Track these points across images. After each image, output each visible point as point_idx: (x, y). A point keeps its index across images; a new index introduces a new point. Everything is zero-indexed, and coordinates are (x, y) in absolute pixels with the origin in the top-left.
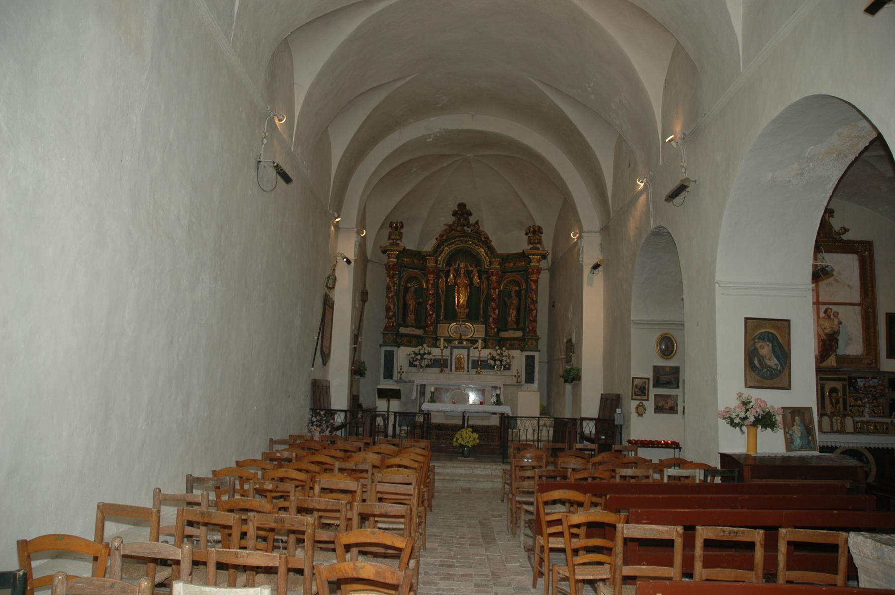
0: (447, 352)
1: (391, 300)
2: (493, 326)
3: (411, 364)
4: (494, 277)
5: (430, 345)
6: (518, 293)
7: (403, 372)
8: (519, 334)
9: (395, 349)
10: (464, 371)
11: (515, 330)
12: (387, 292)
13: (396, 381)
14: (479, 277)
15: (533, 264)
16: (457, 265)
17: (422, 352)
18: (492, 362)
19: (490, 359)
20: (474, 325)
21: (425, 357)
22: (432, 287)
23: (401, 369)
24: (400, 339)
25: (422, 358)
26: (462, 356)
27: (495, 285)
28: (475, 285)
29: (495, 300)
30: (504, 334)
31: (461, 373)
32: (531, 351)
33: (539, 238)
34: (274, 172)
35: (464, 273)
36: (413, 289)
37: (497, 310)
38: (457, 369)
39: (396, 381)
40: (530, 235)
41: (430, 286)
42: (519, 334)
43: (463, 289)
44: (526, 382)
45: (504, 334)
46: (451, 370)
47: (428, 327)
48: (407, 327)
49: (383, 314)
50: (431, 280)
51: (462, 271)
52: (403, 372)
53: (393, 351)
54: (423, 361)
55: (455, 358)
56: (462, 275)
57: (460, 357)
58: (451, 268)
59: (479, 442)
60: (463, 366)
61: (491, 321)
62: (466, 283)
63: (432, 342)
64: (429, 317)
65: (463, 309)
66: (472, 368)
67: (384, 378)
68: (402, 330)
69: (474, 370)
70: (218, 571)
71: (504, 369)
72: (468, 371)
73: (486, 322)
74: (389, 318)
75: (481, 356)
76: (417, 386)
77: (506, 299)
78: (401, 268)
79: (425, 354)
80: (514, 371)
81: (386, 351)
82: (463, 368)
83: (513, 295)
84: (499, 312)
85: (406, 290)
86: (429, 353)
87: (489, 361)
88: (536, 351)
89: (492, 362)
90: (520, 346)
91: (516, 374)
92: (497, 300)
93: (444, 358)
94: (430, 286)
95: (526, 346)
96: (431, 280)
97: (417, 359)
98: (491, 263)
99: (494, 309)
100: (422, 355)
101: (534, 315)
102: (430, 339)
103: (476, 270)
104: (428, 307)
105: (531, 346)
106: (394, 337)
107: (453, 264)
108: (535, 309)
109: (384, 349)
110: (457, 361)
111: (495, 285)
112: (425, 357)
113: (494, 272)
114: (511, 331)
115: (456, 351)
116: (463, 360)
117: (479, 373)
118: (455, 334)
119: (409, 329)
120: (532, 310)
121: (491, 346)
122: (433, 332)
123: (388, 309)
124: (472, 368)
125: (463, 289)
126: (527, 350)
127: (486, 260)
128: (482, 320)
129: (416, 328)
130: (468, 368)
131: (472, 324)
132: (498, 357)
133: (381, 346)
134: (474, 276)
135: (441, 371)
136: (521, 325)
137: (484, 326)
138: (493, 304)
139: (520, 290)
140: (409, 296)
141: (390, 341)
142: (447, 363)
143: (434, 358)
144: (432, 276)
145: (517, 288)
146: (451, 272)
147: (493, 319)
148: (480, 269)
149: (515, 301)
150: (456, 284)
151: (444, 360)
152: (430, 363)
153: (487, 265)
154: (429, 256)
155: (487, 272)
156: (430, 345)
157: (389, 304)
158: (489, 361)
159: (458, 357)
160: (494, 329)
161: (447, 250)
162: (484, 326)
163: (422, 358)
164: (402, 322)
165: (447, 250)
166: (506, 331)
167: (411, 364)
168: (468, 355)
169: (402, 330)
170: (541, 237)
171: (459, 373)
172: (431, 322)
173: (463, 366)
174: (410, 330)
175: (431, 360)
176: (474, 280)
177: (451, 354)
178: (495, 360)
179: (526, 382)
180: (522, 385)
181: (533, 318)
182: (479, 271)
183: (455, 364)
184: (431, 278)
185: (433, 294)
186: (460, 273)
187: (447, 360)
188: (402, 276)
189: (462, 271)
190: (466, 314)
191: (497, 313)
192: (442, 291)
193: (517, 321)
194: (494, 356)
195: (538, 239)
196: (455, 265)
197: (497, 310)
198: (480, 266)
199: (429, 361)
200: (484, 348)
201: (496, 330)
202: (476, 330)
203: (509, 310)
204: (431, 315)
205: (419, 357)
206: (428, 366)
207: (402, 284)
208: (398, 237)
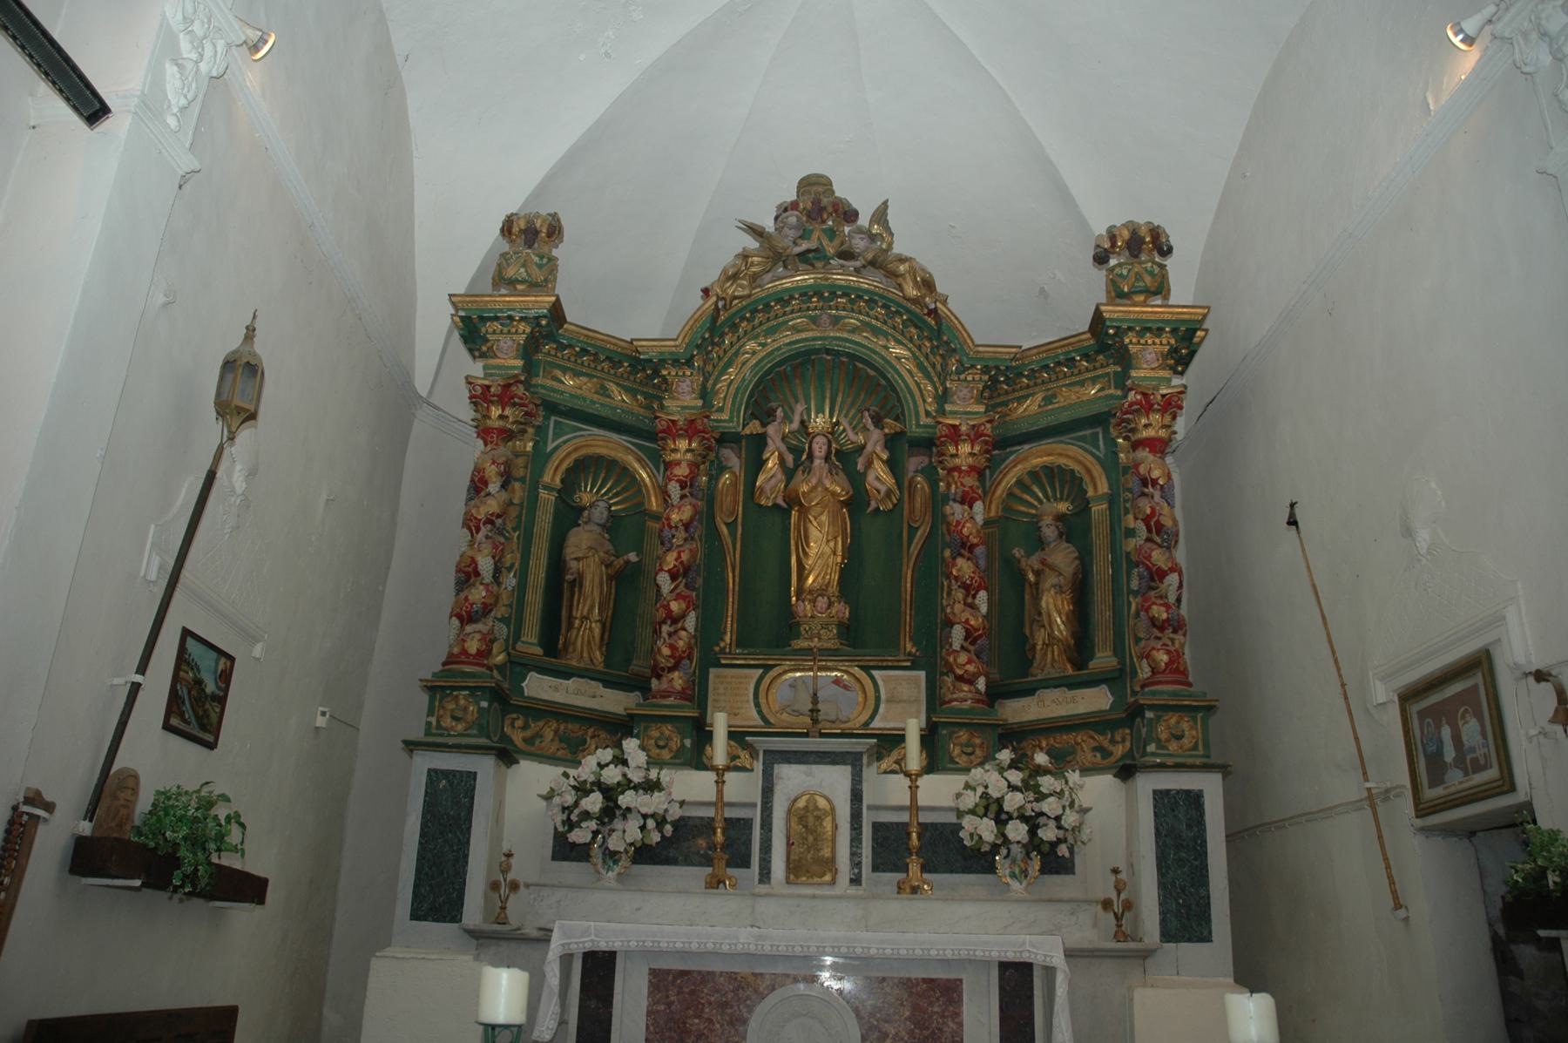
0: (742, 788)
1: (480, 536)
2: (971, 668)
3: (565, 850)
4: (965, 448)
5: (666, 755)
6: (1074, 528)
7: (514, 886)
8: (1097, 700)
9: (484, 767)
10: (833, 882)
11: (1073, 685)
12: (470, 499)
13: (475, 934)
14: (893, 465)
15: (1142, 374)
16: (797, 419)
17: (612, 775)
18: (986, 829)
19: (972, 812)
20: (876, 673)
21: (626, 799)
22: (683, 497)
23: (505, 870)
24: (525, 727)
25: (611, 811)
26: (822, 803)
27: (970, 481)
28: (873, 504)
29: (972, 548)
30: (1020, 711)
31: (818, 892)
32: (1179, 767)
33: (1157, 270)
34: (253, 311)
35: (827, 458)
36: (599, 514)
37: (983, 595)
38: (795, 869)
39: (475, 934)
40: (1113, 262)
41: (674, 489)
42: (1097, 700)
43: (824, 518)
44: (1167, 936)
45: (1020, 711)
46: (765, 875)
47: (659, 677)
48: (566, 674)
49: (445, 595)
50: (678, 463)
51: (819, 447)
52: (514, 886)
53: (472, 776)
54: (618, 824)
55: (789, 812)
56: (817, 462)
57: (811, 807)
58: (771, 429)
59: (550, 251)
60: (826, 853)
61: (956, 646)
62: (834, 494)
63: (675, 743)
64: (665, 629)
65: (822, 602)
66: (875, 868)
67: (416, 916)
68: (538, 686)
69: (889, 875)
70: (995, 973)
71: (1045, 870)
72: (856, 881)
73: (931, 660)
74: (466, 617)
75: (921, 802)
76: (566, 960)
77: (1017, 552)
78: (547, 418)
79: (627, 784)
80: (1093, 875)
81: (434, 775)
82: (830, 864)
83: (1049, 532)
84: (990, 602)
85: (569, 515)
86: (651, 786)
87: (968, 822)
88: (1206, 768)
89: (986, 829)
90: (1106, 754)
91: (1113, 896)
92: (979, 550)
93: (730, 813)
94: (674, 489)
95: (1151, 748)
96: (678, 463)
97: (586, 815)
98: (943, 397)
99: (969, 590)
100: (610, 793)
101: (1172, 598)
102: (667, 729)
103: (876, 435)
104: (664, 580)
105: (1173, 746)
106: (484, 704)
107: (779, 412)
108: (1172, 570)
109: (426, 761)
110: (797, 827)
111: (970, 481)
112: (626, 799)
113: (963, 428)
114: (1050, 695)
115: (792, 779)
116: (827, 824)
117: (915, 890)
118: (785, 716)
119: (572, 683)
120: (1162, 574)
121: (962, 761)
122: (684, 695)
123: (467, 575)
124: (875, 868)
125: (824, 518)
126: (1162, 767)
127: (919, 391)
128: (909, 646)
129: (608, 684)
130: (856, 864)
131: (866, 669)
132: (1014, 801)
133: (411, 746)
134: (869, 464)
135: (715, 883)
136: (1103, 659)
137: (923, 674)
138: (964, 567)
139: (1083, 508)
140: (581, 541)
141: (460, 727)
142: (748, 843)
143: (675, 813)
144: (683, 444)
145: (1063, 507)
146: (771, 446)
147: (969, 635)
148: (898, 426)
149: (1063, 557)
150: (793, 500)
151: (730, 823)
152: (655, 837)
153: (928, 414)
154: (676, 362)
155: (927, 444)
156: (666, 755)
157: (470, 553)
158: (968, 822)
159: (801, 804)
160: (971, 681)
161: (753, 352)
162: (923, 674)
163: (611, 811)
164: (538, 651)
165: (754, 353)
166: (1029, 692)
167: (565, 850)
168: (856, 796)
169: (538, 686)
170: (1162, 267)
171: (809, 891)
172: (672, 647)
173: (826, 853)
174: (578, 693)
175: (661, 821)
176: (871, 477)
177: (768, 791)
178: (1001, 819)
179: (1167, 936)
180: (1146, 955)
181: (1167, 606)
182: (891, 442)
183: (789, 845)
184: (678, 456)
185: (687, 526)
186: (811, 457)
187: (748, 823)
188: (550, 447)
189: (819, 447)
190: (840, 625)
191: (984, 609)
192: (731, 526)
193: (1080, 649)
194: (995, 794)
195: (1151, 274)
196: (788, 419)
197: (983, 595)
198: (897, 419)
199: (651, 823)
200: (931, 767)
201: (981, 684)
202: (883, 696)
203: (1037, 598)
204: (676, 620)
205: (594, 802)
206: (644, 854)
207: (547, 478)
208: (535, 271)
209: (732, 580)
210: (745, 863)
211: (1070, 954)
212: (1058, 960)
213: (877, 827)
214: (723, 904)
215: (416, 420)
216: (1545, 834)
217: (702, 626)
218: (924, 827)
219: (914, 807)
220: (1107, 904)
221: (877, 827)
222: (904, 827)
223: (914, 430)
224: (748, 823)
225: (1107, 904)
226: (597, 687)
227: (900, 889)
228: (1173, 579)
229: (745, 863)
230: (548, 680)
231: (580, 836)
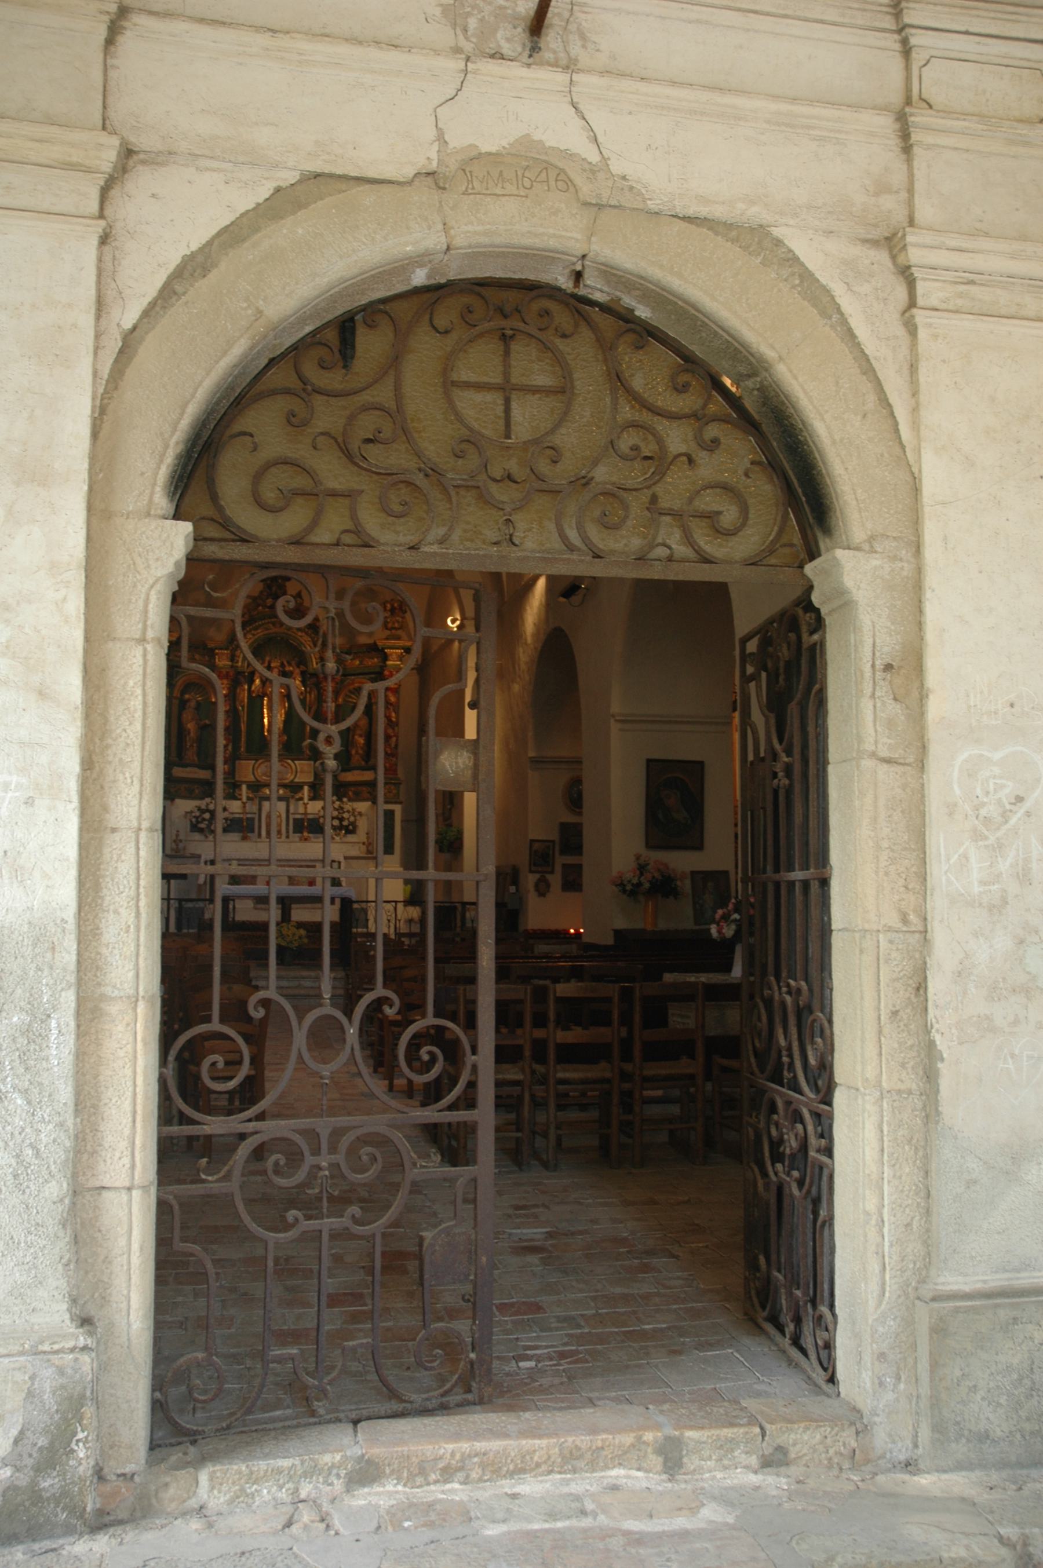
36: (193, 704)
44: (310, 800)
46: (260, 835)
48: (186, 766)
72: (288, 837)
97: (204, 819)
117: (306, 839)
119: (189, 769)
130: (288, 832)
135: (244, 838)
168: (288, 811)
177: (260, 810)
179: (310, 800)
187: (253, 819)
209: (243, 727)
210: (252, 831)
211: (346, 858)
212: (342, 859)
213: (295, 820)
214: (246, 845)
215: (253, 762)
216: (816, 637)
217: (233, 748)
218: (309, 820)
219: (306, 814)
220: (364, 843)
221: (295, 820)
222: (302, 820)
223: (311, 671)
224: (253, 819)
225: (364, 843)
226: (196, 769)
227: (301, 840)
228: (394, 739)
229: (252, 831)
230: (181, 769)
231: (202, 826)
